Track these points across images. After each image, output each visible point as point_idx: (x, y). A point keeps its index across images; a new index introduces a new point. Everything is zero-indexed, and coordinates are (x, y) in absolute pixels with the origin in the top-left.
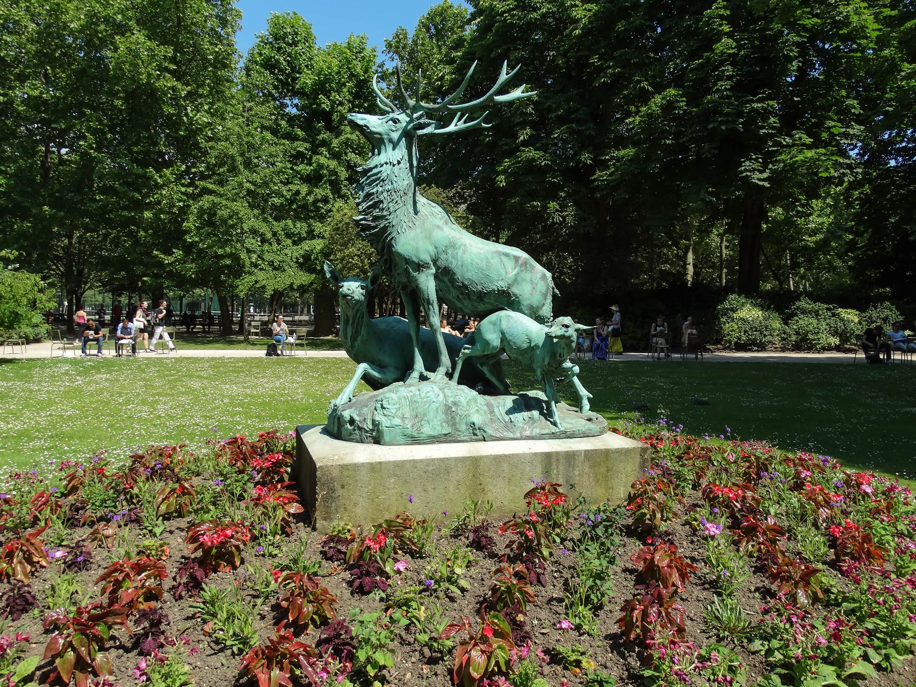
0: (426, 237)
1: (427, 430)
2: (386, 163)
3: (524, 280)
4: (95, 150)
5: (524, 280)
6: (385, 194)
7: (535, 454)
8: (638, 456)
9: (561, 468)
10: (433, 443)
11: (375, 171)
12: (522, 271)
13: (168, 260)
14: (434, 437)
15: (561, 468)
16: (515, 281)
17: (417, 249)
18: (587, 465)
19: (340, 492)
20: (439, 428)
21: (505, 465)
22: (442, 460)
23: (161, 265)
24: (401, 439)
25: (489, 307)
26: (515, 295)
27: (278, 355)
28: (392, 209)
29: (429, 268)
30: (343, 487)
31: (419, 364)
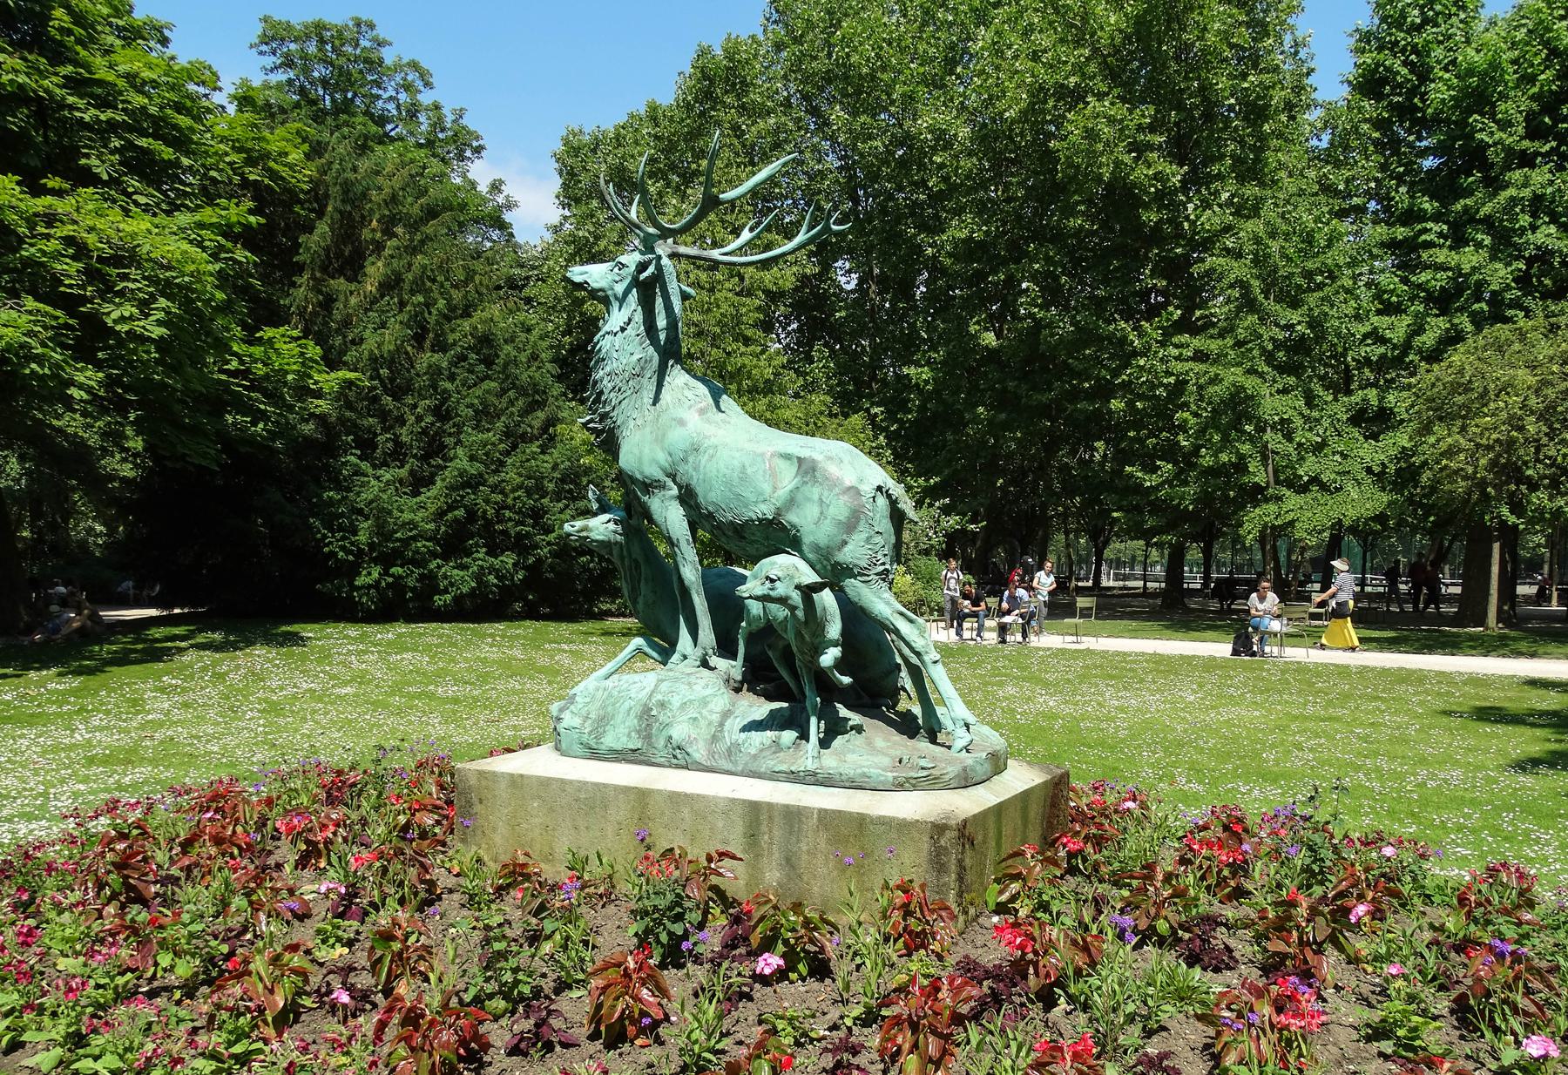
0: (656, 440)
1: (610, 741)
3: (809, 500)
4: (1041, 307)
5: (809, 500)
7: (733, 800)
8: (926, 839)
9: (777, 833)
10: (617, 760)
12: (805, 483)
13: (1150, 481)
14: (617, 752)
15: (777, 833)
16: (791, 502)
17: (640, 459)
18: (822, 838)
19: (478, 808)
20: (625, 739)
21: (686, 812)
22: (598, 786)
23: (1138, 488)
24: (578, 749)
27: (1254, 654)
29: (663, 487)
30: (481, 802)
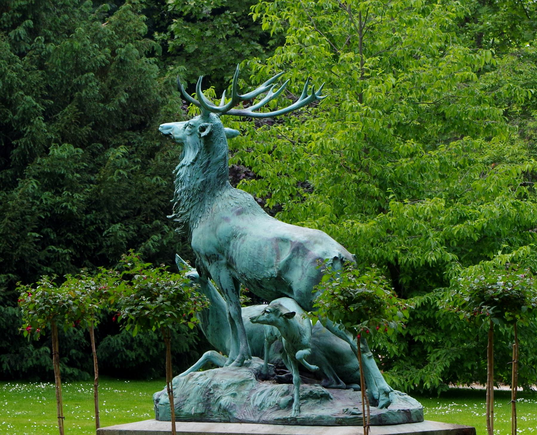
3: (297, 265)
16: (287, 267)
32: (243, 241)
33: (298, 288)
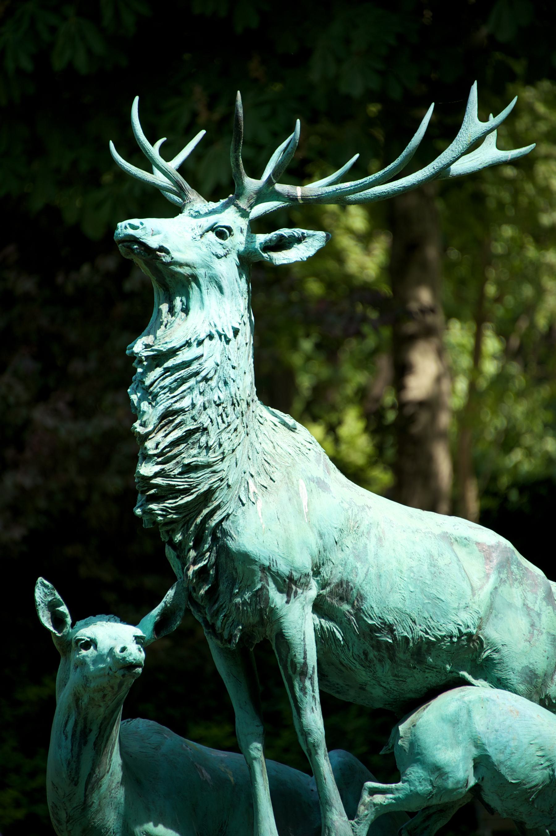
2: (211, 337)
3: (510, 605)
6: (212, 411)
11: (184, 356)
12: (502, 581)
17: (288, 542)
25: (432, 679)
26: (492, 645)
28: (227, 446)
31: (419, 757)
32: (380, 539)
33: (525, 663)
